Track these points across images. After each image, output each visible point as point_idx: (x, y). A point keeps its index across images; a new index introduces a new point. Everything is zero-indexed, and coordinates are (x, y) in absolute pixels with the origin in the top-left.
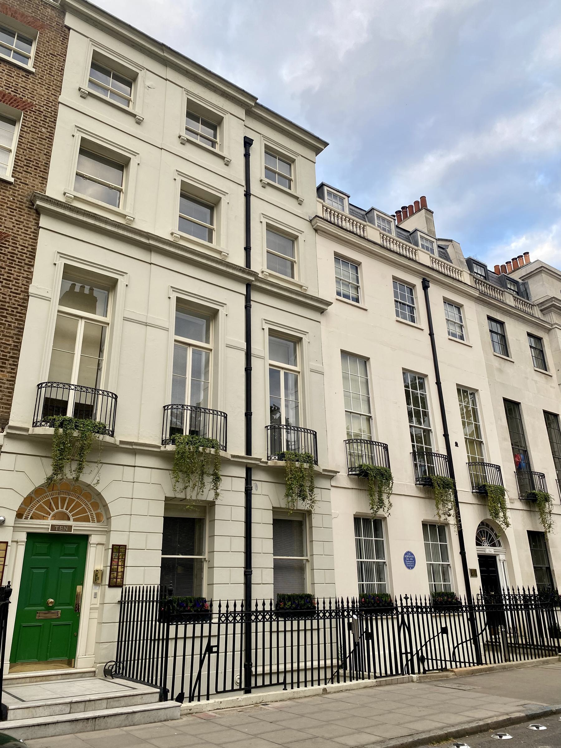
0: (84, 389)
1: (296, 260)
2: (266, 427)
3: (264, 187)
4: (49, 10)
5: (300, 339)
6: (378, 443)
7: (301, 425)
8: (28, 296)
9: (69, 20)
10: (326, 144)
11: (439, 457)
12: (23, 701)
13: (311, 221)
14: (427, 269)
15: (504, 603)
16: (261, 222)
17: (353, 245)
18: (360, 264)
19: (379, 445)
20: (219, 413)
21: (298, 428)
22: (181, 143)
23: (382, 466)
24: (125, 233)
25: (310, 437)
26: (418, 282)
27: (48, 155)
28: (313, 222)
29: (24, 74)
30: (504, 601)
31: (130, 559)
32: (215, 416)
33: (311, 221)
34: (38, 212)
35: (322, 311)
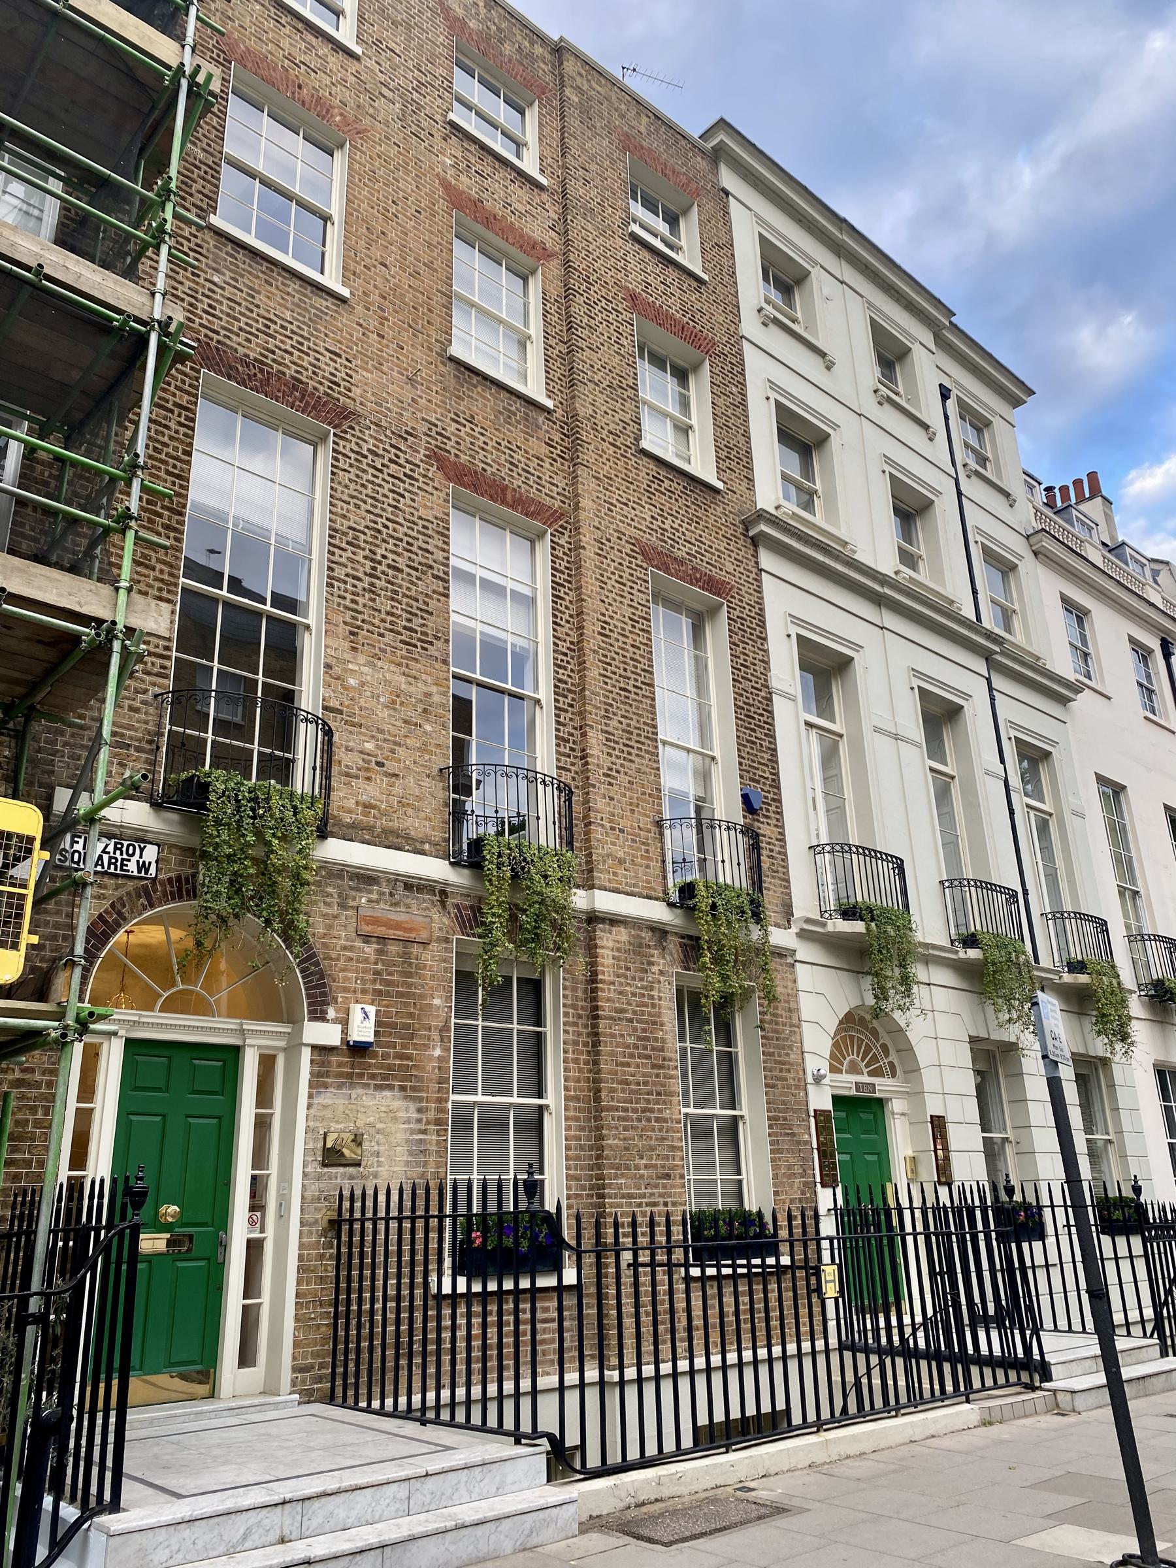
0: (838, 848)
1: (1016, 607)
2: (942, 882)
3: (880, 403)
4: (699, 159)
5: (1048, 755)
6: (875, 851)
7: (1068, 906)
8: (771, 693)
9: (728, 179)
10: (1031, 392)
11: (991, 890)
12: (179, 1496)
13: (1028, 537)
14: (1162, 616)
15: (739, 1262)
16: (768, 398)
17: (1073, 574)
18: (1087, 612)
19: (882, 860)
20: (854, 849)
21: (960, 881)
22: (879, 403)
23: (890, 904)
24: (820, 557)
25: (885, 868)
26: (1154, 644)
27: (747, 436)
28: (1033, 540)
29: (695, 284)
30: (744, 1262)
31: (952, 1131)
32: (847, 855)
33: (1028, 537)
34: (755, 542)
35: (1064, 701)
